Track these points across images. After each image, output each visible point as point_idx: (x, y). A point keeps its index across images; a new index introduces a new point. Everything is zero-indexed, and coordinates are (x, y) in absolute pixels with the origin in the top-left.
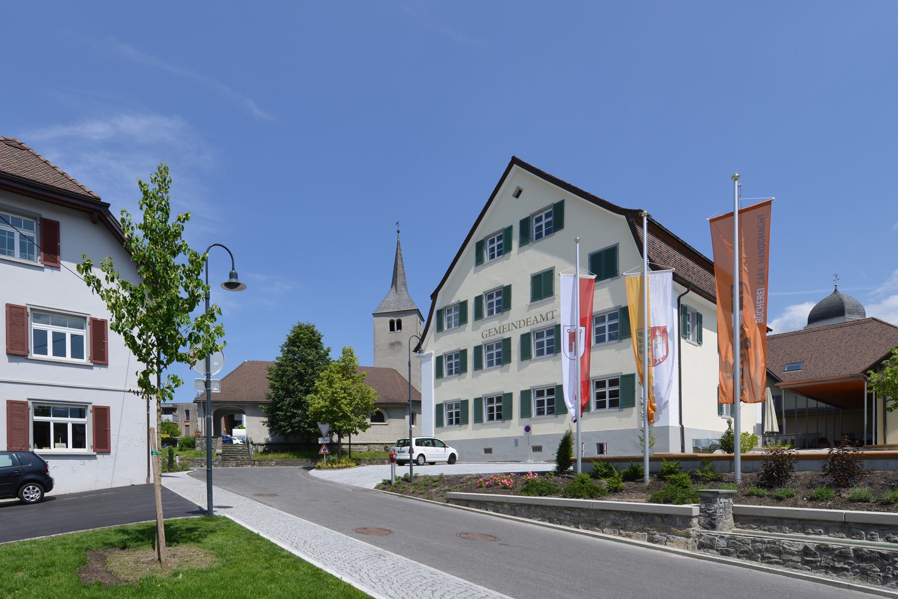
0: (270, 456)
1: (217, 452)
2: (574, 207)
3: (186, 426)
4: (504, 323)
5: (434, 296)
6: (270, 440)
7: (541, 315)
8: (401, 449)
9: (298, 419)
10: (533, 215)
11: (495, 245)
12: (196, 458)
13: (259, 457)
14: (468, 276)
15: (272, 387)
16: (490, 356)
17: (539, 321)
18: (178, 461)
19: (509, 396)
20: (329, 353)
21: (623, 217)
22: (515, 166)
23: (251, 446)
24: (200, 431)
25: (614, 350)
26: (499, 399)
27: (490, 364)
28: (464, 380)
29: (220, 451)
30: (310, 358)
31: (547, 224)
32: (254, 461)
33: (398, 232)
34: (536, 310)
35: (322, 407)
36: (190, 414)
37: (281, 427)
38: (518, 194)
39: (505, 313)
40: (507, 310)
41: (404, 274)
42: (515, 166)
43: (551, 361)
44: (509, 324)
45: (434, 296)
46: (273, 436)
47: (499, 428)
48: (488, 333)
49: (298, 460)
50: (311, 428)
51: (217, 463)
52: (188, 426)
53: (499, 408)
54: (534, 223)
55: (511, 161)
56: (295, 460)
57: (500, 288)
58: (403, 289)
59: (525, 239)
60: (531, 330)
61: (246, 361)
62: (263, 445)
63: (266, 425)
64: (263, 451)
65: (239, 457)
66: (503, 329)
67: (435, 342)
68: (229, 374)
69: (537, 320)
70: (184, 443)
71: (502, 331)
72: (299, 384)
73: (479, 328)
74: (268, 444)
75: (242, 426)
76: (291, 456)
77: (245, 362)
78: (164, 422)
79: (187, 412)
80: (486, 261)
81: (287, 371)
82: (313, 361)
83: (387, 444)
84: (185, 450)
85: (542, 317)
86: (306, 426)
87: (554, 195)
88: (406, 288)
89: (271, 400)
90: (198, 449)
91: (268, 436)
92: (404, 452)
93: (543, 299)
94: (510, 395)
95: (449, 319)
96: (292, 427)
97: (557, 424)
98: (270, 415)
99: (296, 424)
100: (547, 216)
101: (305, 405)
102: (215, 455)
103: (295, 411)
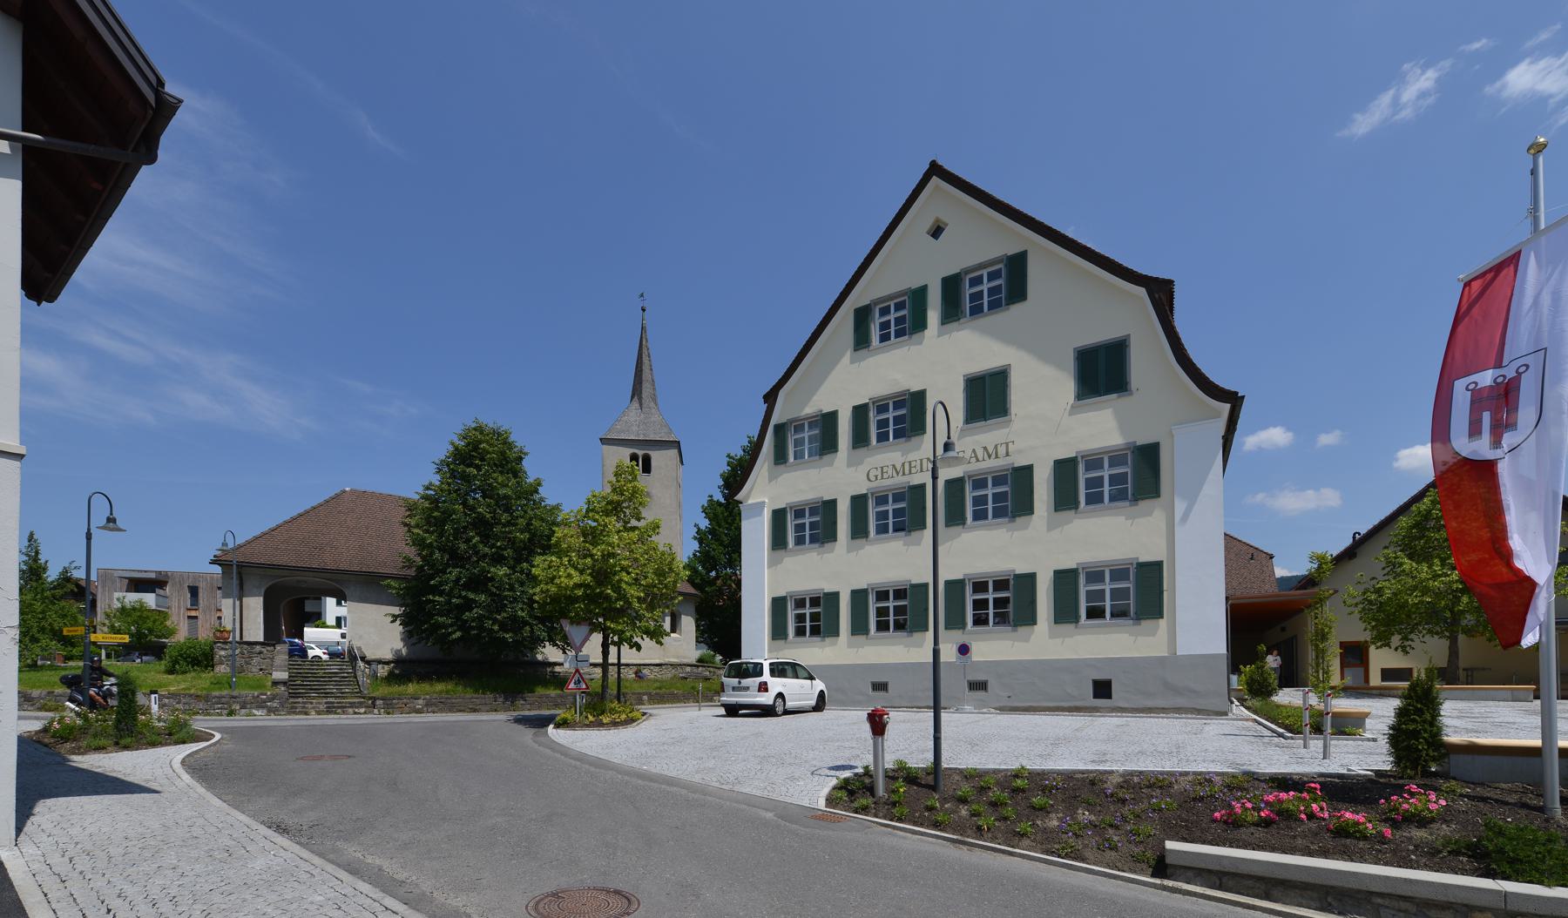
0: (411, 688)
1: (274, 677)
2: (1045, 263)
3: (189, 617)
4: (911, 457)
5: (771, 398)
6: (404, 653)
7: (985, 448)
8: (740, 683)
9: (476, 612)
10: (968, 271)
11: (892, 317)
12: (217, 693)
13: (384, 690)
14: (839, 367)
15: (419, 543)
16: (800, 528)
17: (981, 459)
18: (155, 708)
19: (834, 597)
20: (540, 489)
21: (1141, 291)
22: (935, 180)
23: (361, 664)
24: (229, 627)
25: (1124, 517)
26: (815, 601)
27: (800, 541)
28: (831, 554)
29: (282, 675)
30: (502, 492)
31: (992, 291)
32: (374, 699)
33: (644, 310)
34: (977, 438)
35: (578, 586)
36: (200, 595)
37: (439, 626)
38: (937, 232)
39: (913, 439)
40: (918, 435)
41: (653, 381)
42: (935, 180)
43: (1005, 530)
44: (921, 460)
45: (771, 398)
46: (413, 644)
47: (902, 646)
48: (879, 473)
49: (476, 696)
50: (506, 631)
51: (275, 705)
52: (196, 617)
53: (815, 617)
54: (967, 287)
55: (928, 170)
56: (468, 696)
57: (903, 393)
58: (652, 404)
59: (952, 313)
60: (964, 473)
61: (347, 489)
62: (387, 663)
63: (398, 622)
64: (389, 675)
65: (332, 688)
66: (910, 467)
67: (770, 481)
68: (307, 512)
69: (976, 456)
70: (181, 655)
71: (907, 471)
72: (482, 542)
73: (861, 463)
74: (398, 661)
75: (324, 623)
76: (460, 688)
77: (344, 492)
78: (128, 606)
79: (194, 591)
80: (874, 344)
81: (454, 512)
82: (510, 498)
83: (640, 665)
84: (184, 672)
85: (896, 470)
86: (496, 627)
87: (1011, 239)
88: (656, 404)
89: (412, 572)
90: (222, 669)
91: (399, 645)
92: (747, 689)
93: (989, 419)
94: (1031, 578)
95: (798, 443)
96: (463, 626)
97: (1016, 643)
98: (409, 601)
99: (473, 621)
100: (993, 276)
101: (493, 586)
102: (270, 683)
103: (472, 596)
